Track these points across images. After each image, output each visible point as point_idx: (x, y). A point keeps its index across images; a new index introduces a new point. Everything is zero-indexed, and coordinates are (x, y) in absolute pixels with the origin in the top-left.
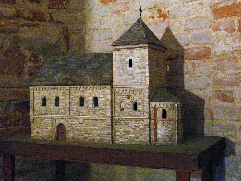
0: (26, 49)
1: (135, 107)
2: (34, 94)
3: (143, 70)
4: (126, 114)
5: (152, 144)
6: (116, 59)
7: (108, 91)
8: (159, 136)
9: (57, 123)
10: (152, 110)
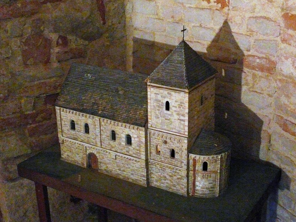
0: (51, 31)
1: (173, 154)
2: (60, 115)
3: (182, 118)
4: (163, 159)
5: (190, 194)
6: (152, 97)
7: (142, 133)
8: (197, 188)
9: (88, 152)
10: (191, 162)
